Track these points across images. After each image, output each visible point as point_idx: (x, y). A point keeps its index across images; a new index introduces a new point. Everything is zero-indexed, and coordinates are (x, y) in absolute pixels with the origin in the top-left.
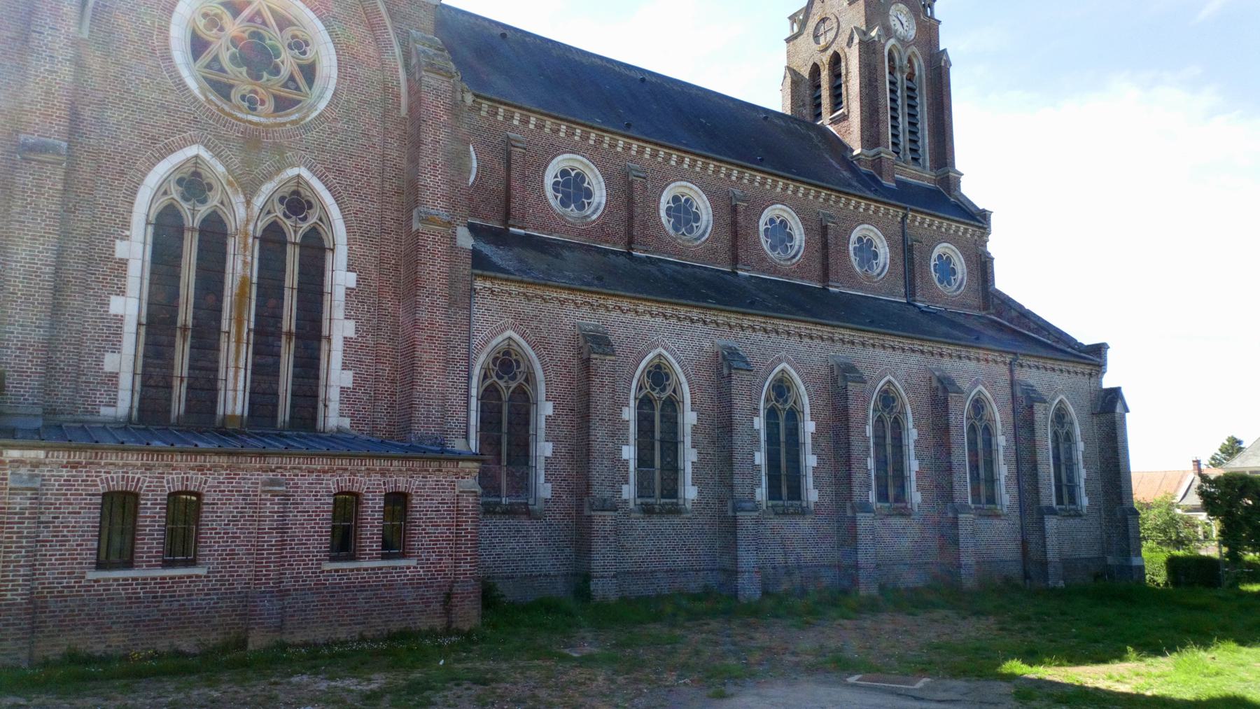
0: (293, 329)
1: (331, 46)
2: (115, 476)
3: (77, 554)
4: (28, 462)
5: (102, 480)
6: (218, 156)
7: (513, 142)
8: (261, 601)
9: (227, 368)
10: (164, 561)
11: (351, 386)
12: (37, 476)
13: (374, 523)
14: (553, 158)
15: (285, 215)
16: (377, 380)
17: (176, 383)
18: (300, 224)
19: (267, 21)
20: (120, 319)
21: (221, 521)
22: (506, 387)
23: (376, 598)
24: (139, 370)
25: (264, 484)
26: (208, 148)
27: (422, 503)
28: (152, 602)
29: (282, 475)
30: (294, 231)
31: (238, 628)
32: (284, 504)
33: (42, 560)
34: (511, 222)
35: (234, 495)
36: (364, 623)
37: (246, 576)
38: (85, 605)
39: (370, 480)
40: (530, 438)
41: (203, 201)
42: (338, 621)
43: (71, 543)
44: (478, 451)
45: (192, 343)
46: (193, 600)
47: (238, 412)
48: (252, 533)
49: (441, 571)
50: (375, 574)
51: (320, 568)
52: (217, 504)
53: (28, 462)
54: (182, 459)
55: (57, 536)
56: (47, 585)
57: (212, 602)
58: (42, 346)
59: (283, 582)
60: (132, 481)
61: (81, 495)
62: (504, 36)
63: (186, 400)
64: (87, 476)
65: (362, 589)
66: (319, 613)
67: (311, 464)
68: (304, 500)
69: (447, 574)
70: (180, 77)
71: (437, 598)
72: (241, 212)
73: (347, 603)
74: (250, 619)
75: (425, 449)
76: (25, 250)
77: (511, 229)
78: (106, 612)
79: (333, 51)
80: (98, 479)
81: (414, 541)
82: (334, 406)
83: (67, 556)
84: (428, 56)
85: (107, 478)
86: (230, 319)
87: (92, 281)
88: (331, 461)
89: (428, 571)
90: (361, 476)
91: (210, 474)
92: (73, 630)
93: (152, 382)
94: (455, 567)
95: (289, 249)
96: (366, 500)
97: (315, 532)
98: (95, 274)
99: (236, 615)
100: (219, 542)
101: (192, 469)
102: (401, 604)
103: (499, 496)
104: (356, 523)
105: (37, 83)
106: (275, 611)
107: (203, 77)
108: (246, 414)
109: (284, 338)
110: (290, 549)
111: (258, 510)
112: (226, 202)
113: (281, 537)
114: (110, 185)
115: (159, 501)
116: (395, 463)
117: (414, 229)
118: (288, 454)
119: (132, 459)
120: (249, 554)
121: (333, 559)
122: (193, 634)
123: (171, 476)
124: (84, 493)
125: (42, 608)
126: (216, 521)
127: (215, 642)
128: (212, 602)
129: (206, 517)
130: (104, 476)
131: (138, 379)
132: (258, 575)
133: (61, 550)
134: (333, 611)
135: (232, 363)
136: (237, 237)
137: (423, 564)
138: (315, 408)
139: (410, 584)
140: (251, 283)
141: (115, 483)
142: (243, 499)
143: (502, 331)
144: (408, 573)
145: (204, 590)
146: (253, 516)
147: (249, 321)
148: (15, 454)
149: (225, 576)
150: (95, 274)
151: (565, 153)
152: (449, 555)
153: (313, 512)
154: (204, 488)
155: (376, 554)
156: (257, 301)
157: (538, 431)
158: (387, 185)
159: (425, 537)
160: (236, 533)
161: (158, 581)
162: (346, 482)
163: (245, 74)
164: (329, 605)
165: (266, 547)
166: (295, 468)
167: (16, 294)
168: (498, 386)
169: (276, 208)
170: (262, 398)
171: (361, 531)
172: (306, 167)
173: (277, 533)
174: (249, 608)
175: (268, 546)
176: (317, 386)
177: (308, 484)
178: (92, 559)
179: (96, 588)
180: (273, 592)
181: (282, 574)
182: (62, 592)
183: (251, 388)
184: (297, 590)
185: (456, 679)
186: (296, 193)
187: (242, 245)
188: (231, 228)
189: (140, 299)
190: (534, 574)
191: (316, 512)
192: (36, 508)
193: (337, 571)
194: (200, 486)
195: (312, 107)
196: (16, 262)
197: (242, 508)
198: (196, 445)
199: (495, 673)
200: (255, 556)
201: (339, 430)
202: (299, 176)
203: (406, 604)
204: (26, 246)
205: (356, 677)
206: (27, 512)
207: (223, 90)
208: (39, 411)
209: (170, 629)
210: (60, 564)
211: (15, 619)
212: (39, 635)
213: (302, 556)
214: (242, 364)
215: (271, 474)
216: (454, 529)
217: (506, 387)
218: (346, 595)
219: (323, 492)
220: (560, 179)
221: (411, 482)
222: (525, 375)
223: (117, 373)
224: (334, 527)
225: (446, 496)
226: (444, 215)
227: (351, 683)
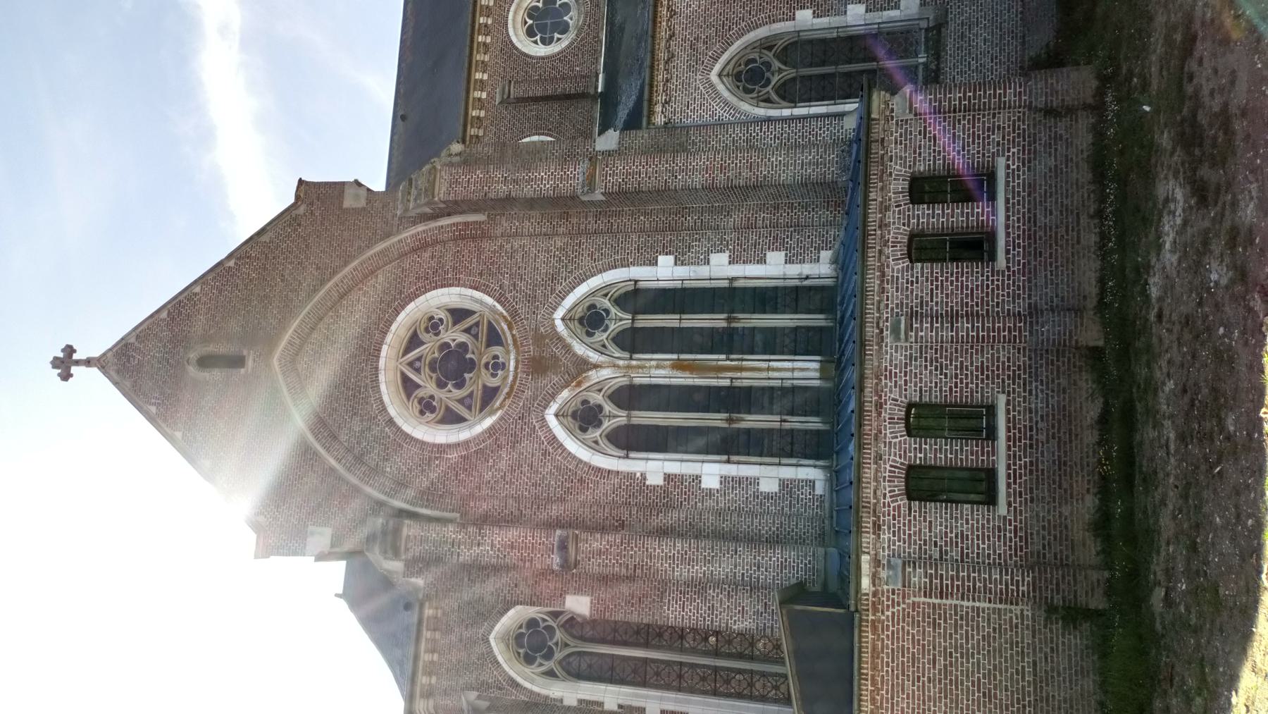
0: (724, 316)
1: (429, 295)
2: (888, 489)
3: (978, 523)
4: (874, 570)
5: (893, 502)
6: (553, 397)
7: (505, 97)
8: (1042, 335)
9: (769, 379)
10: (988, 438)
11: (783, 253)
12: (889, 561)
13: (948, 214)
14: (517, 49)
15: (605, 331)
16: (777, 226)
17: (787, 426)
18: (612, 315)
19: (418, 356)
20: (724, 480)
21: (941, 382)
22: (780, 73)
23: (1045, 202)
24: (776, 460)
25: (897, 338)
26: (547, 406)
27: (924, 159)
28: (1037, 449)
29: (887, 322)
30: (620, 320)
31: (1074, 357)
32: (922, 317)
33: (984, 556)
34: (592, 91)
35: (911, 370)
36: (1078, 214)
37: (1009, 353)
38: (1037, 515)
39: (894, 223)
40: (842, 35)
41: (600, 408)
42: (1073, 245)
43: (964, 529)
44: (858, 100)
45: (745, 413)
46: (1036, 408)
47: (816, 365)
48: (956, 349)
49: (1014, 126)
50: (1014, 207)
51: (1003, 272)
52: (921, 387)
53: (874, 570)
54: (868, 425)
55: (957, 543)
56: (1013, 552)
57: (1040, 387)
58: (755, 549)
59: (1019, 312)
60: (895, 472)
61: (910, 521)
62: (403, 118)
63: (805, 416)
64: (889, 515)
65: (1033, 220)
66: (1061, 268)
67: (873, 291)
68: (917, 295)
69: (1019, 117)
70: (483, 433)
71: (1050, 127)
72: (606, 373)
73: (1051, 236)
74: (1065, 345)
75: (855, 161)
76: (662, 564)
77: (599, 90)
78: (1046, 494)
79: (434, 292)
80: (892, 505)
81: (973, 164)
82: (807, 269)
83: (980, 533)
84: (419, 195)
85: (891, 497)
86: (718, 378)
87: (689, 504)
88: (870, 269)
89: (1014, 141)
90: (889, 234)
91: (886, 396)
92: (1066, 527)
93: (788, 448)
94: (1010, 107)
95: (639, 324)
96: (918, 225)
97: (957, 281)
98: (681, 502)
99: (1058, 361)
100: (967, 384)
101: (879, 414)
102: (1056, 171)
103: (916, 67)
104: (947, 235)
105: (505, 556)
106: (1056, 319)
107: (481, 410)
108: (818, 358)
109: (734, 325)
110: (977, 306)
111: (929, 344)
112: (599, 387)
113: (962, 317)
114: (594, 490)
115: (917, 446)
116: (872, 196)
117: (602, 198)
118: (862, 317)
119: (869, 473)
120: (982, 351)
121: (993, 257)
122: (1078, 406)
123: (888, 435)
124: (908, 518)
125: (1038, 556)
126: (941, 387)
127: (1090, 382)
128: (1040, 387)
129: (936, 397)
130: (888, 499)
131: (784, 461)
132: (1010, 339)
133: (973, 539)
134: (1060, 251)
135: (764, 375)
136: (632, 375)
137: (1003, 150)
138: (810, 288)
139: (1029, 162)
140: (678, 359)
141: (896, 489)
142: (916, 360)
143: (712, 85)
144: (1015, 167)
145: (1025, 397)
146: (936, 350)
147: (718, 360)
148: (866, 583)
149: (1009, 376)
150: (681, 502)
151: (508, 35)
152: (994, 117)
153: (932, 285)
154: (901, 402)
155: (988, 207)
156: (697, 353)
157: (833, 26)
158: (561, 230)
159: (968, 151)
160: (956, 366)
161: (1011, 443)
162: (896, 251)
163: (471, 375)
164: (1051, 257)
165: (975, 334)
166: (879, 309)
167: (705, 571)
168: (778, 84)
169: (599, 339)
170: (799, 343)
171: (957, 228)
172: (553, 313)
173: (957, 322)
174: (1050, 348)
175: (972, 332)
176: (785, 288)
177: (897, 292)
178: (983, 509)
179: (1018, 505)
180: (1031, 323)
181: (1009, 314)
182: (1021, 537)
183: (790, 354)
184: (1030, 296)
185: (1181, 79)
186: (581, 321)
187: (640, 370)
188: (624, 381)
189: (703, 462)
190: (1020, 9)
191: (932, 281)
192: (925, 563)
193: (1008, 252)
194: (899, 406)
195: (493, 310)
196: (673, 571)
197: (926, 361)
198: (853, 411)
199: (1174, 28)
200: (985, 345)
201: (834, 261)
202: (563, 319)
203: (1056, 166)
204: (658, 563)
205: (1161, 216)
206: (929, 571)
207: (490, 394)
208: (821, 551)
209: (1071, 430)
210: (989, 540)
211: (1051, 584)
212: (1071, 560)
213: (988, 293)
214: (764, 365)
215: (885, 333)
216: (959, 115)
217: (780, 73)
218: (1040, 239)
219: (907, 275)
220: (538, 38)
221: (896, 175)
222: (763, 51)
223: (780, 480)
224: (953, 259)
225: (916, 129)
226: (583, 167)
227: (1169, 229)
